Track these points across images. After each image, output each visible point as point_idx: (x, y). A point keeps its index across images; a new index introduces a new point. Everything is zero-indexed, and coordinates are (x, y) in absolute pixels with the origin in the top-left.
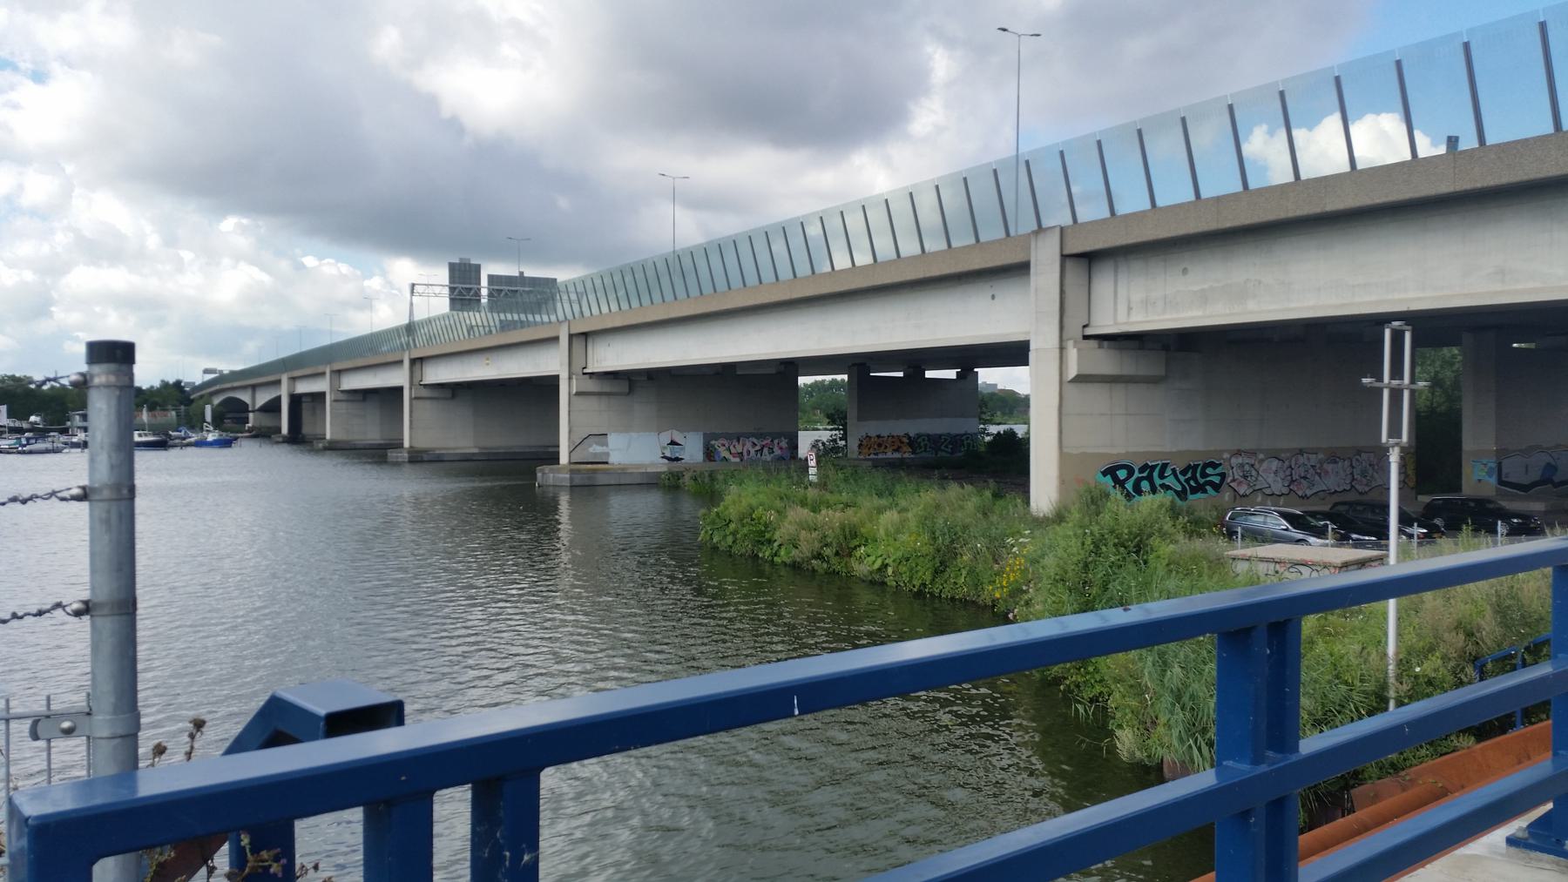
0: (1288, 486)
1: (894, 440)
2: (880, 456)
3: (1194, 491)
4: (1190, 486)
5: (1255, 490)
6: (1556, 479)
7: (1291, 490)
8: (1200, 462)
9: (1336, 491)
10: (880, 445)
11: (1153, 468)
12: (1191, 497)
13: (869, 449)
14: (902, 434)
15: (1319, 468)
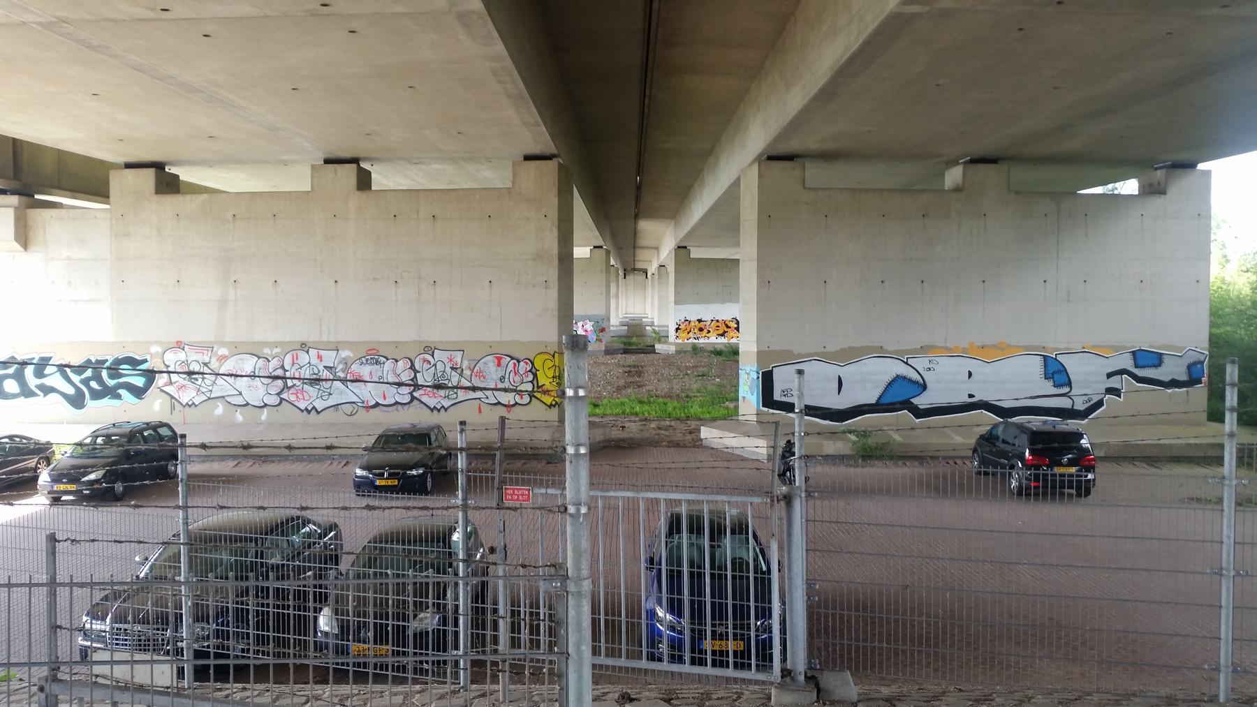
0: (278, 394)
1: (718, 324)
2: (702, 341)
3: (96, 395)
4: (91, 389)
5: (209, 398)
6: (922, 401)
7: (282, 399)
8: (108, 357)
9: (377, 405)
10: (701, 330)
11: (24, 364)
12: (90, 403)
13: (688, 333)
14: (730, 319)
15: (343, 371)
